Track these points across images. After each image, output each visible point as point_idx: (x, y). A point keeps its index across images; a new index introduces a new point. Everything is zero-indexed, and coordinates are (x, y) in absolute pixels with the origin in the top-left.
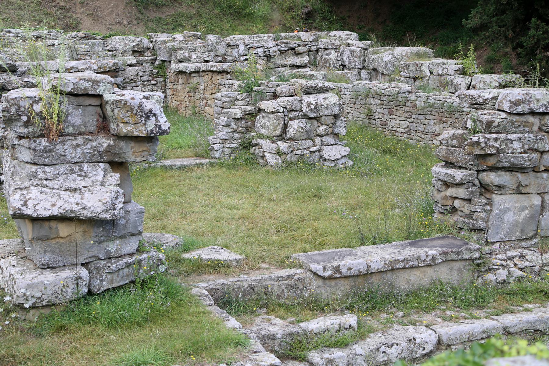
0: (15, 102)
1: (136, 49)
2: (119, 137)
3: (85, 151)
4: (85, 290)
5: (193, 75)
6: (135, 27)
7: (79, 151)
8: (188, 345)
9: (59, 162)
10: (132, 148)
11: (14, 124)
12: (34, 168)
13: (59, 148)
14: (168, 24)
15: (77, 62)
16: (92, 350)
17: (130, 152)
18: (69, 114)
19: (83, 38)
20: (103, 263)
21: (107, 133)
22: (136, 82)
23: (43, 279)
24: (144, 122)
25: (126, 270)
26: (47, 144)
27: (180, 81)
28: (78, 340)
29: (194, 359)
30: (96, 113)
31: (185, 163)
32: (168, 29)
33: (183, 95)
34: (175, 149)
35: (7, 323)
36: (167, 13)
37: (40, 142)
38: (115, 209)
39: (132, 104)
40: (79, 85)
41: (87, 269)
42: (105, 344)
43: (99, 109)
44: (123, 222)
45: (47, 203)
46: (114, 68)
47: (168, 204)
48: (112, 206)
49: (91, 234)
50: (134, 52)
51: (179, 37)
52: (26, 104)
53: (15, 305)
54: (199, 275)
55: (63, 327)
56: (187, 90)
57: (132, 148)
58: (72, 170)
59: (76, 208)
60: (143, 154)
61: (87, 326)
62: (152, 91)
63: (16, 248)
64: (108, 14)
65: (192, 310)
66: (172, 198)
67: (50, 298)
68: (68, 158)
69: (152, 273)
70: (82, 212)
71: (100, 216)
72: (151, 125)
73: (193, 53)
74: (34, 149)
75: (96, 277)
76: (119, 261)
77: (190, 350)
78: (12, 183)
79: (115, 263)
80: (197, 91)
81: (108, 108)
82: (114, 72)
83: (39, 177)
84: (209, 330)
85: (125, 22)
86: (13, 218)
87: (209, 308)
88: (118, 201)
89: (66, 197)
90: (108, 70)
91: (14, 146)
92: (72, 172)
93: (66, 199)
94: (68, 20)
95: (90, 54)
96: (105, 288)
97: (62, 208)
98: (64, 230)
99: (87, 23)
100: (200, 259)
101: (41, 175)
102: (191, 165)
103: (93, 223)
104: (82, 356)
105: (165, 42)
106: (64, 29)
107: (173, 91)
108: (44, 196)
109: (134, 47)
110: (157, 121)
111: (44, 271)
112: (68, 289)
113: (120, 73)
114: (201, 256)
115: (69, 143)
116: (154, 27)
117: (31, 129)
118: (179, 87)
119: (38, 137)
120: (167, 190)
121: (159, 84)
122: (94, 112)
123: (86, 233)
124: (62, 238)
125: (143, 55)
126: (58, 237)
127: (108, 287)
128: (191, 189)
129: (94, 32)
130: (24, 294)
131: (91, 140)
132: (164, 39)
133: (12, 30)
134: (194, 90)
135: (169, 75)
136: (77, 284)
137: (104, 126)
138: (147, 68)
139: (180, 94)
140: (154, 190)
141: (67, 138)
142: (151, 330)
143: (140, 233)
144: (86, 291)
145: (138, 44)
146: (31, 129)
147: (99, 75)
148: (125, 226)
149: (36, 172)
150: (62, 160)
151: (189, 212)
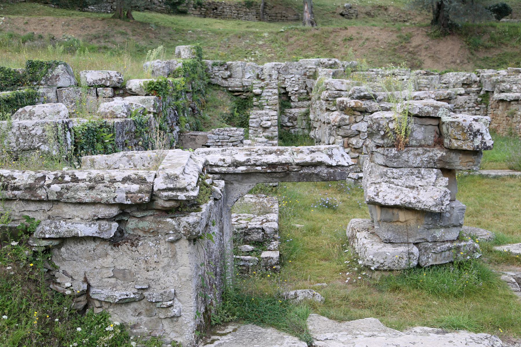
0: (377, 121)
1: (465, 82)
2: (450, 150)
3: (424, 159)
4: (415, 263)
5: (512, 103)
6: (466, 65)
7: (419, 159)
8: (496, 320)
9: (404, 166)
10: (460, 159)
11: (374, 137)
12: (385, 169)
13: (405, 156)
14: (494, 62)
15: (420, 92)
16: (418, 308)
17: (458, 162)
18: (414, 131)
19: (424, 74)
20: (430, 244)
21: (441, 147)
22: (464, 108)
23: (385, 251)
24: (472, 139)
25: (447, 253)
26: (396, 152)
27: (500, 108)
28: (408, 299)
29: (501, 331)
30: (435, 131)
31: (500, 174)
32: (494, 66)
33: (502, 119)
34: (491, 162)
35: (360, 278)
36: (494, 53)
37: (391, 151)
38: (443, 205)
39: (464, 125)
40: (424, 109)
41: (418, 247)
42: (429, 306)
43: (437, 128)
44: (448, 215)
45: (392, 195)
46: (448, 96)
47: (483, 206)
48: (441, 202)
49: (423, 222)
50: (463, 84)
51: (503, 72)
52: (383, 123)
53: (365, 266)
54: (508, 265)
55: (397, 288)
56: (506, 114)
57: (460, 159)
58: (412, 173)
59: (413, 201)
60: (468, 164)
61: (415, 290)
62: (476, 115)
63: (367, 226)
64: (445, 55)
65: (500, 292)
66: (487, 201)
67: (390, 265)
68: (410, 164)
69: (468, 257)
70: (418, 204)
71: (431, 209)
72: (477, 142)
73: (514, 85)
74: (387, 156)
75: (424, 255)
76: (442, 245)
77: (498, 324)
78: (369, 178)
79: (439, 246)
80: (515, 116)
81: (444, 128)
82: (448, 99)
83: (388, 176)
84: (515, 311)
85: (458, 61)
86: (368, 204)
87: (516, 294)
88: (446, 199)
89: (406, 192)
90: (443, 98)
91: (372, 153)
92: (412, 174)
93: (407, 194)
94: (414, 61)
95: (428, 86)
96: (430, 264)
97: (403, 200)
98: (402, 216)
99: (428, 63)
100: (509, 253)
101: (390, 174)
102: (505, 175)
103: (425, 214)
104: (411, 312)
105: (491, 76)
106: (410, 68)
107: (493, 115)
108: (391, 190)
109: (464, 80)
110: (483, 138)
111: (386, 244)
112: (403, 260)
113: (452, 101)
114: (511, 251)
115: (412, 152)
116: (482, 64)
117: (386, 141)
118: (499, 113)
119: (390, 147)
120: (482, 194)
121: (482, 110)
122: (432, 130)
123: (419, 221)
124: (401, 222)
125: (471, 87)
126: (398, 221)
127: (432, 264)
128: (504, 195)
129: (434, 70)
130: (372, 259)
131: (429, 151)
132: (490, 74)
133: (374, 70)
134: (513, 115)
135: (491, 102)
136: (410, 258)
137: (439, 141)
138: (473, 96)
139: (499, 118)
140: (472, 193)
141: (411, 148)
142: (465, 302)
143: (461, 225)
144: (416, 264)
145: (467, 79)
146: (386, 141)
147: (439, 102)
148: (449, 218)
149: (387, 172)
150: (406, 165)
151: (501, 213)
